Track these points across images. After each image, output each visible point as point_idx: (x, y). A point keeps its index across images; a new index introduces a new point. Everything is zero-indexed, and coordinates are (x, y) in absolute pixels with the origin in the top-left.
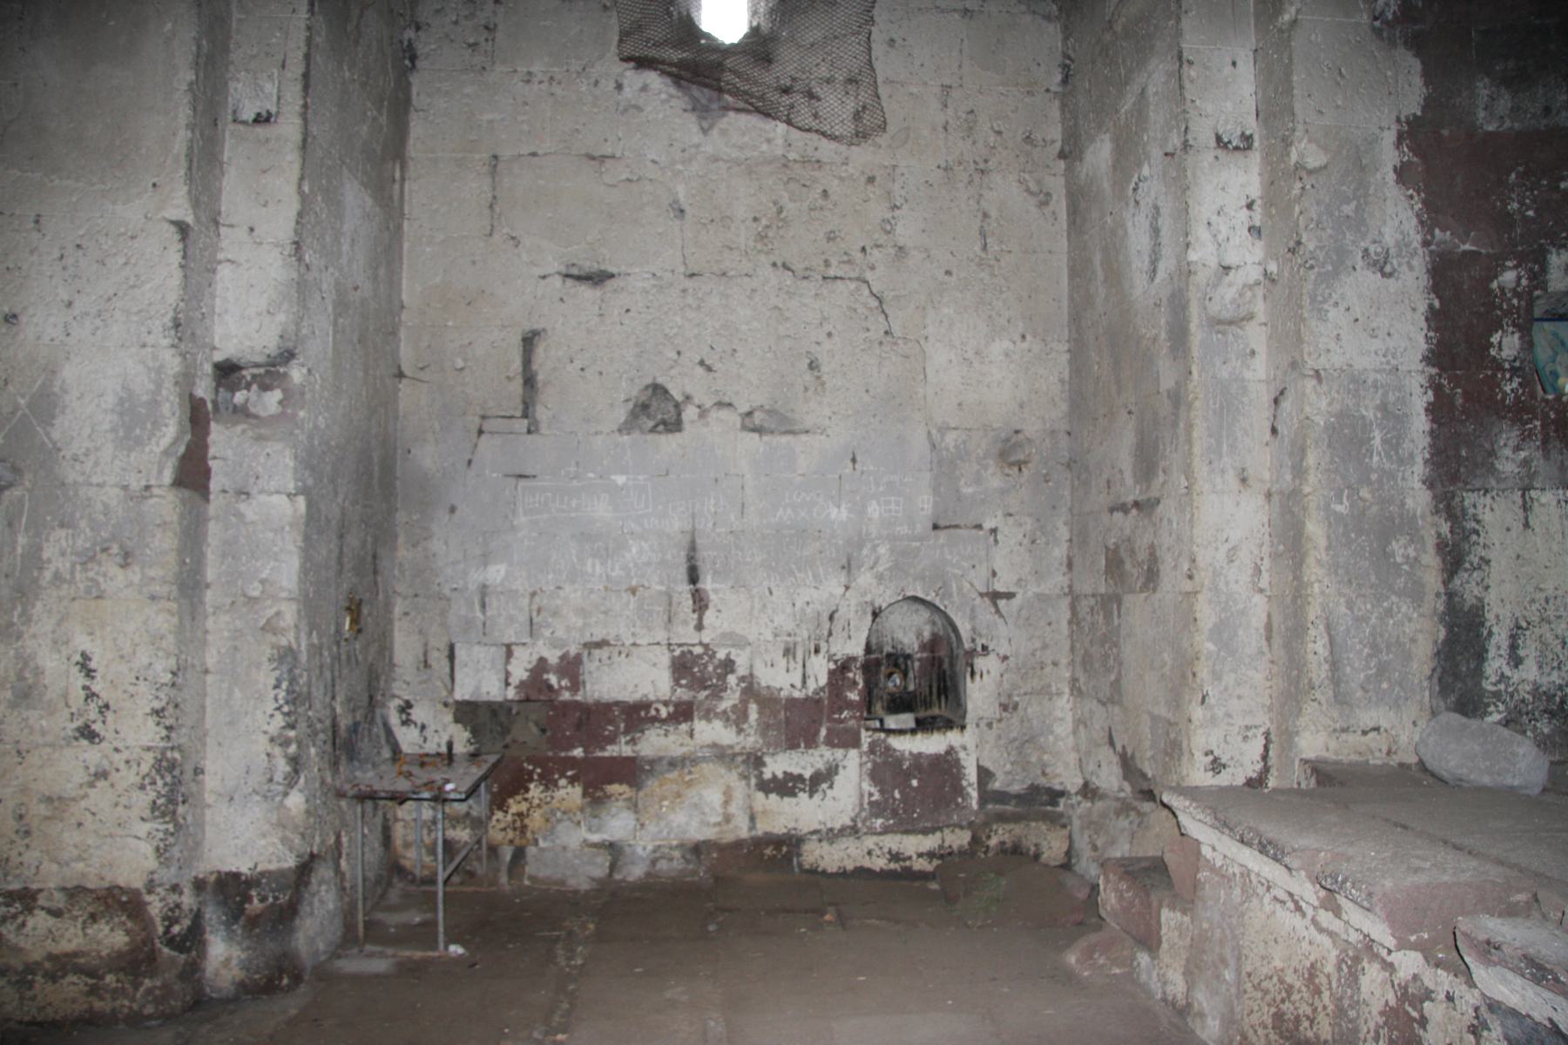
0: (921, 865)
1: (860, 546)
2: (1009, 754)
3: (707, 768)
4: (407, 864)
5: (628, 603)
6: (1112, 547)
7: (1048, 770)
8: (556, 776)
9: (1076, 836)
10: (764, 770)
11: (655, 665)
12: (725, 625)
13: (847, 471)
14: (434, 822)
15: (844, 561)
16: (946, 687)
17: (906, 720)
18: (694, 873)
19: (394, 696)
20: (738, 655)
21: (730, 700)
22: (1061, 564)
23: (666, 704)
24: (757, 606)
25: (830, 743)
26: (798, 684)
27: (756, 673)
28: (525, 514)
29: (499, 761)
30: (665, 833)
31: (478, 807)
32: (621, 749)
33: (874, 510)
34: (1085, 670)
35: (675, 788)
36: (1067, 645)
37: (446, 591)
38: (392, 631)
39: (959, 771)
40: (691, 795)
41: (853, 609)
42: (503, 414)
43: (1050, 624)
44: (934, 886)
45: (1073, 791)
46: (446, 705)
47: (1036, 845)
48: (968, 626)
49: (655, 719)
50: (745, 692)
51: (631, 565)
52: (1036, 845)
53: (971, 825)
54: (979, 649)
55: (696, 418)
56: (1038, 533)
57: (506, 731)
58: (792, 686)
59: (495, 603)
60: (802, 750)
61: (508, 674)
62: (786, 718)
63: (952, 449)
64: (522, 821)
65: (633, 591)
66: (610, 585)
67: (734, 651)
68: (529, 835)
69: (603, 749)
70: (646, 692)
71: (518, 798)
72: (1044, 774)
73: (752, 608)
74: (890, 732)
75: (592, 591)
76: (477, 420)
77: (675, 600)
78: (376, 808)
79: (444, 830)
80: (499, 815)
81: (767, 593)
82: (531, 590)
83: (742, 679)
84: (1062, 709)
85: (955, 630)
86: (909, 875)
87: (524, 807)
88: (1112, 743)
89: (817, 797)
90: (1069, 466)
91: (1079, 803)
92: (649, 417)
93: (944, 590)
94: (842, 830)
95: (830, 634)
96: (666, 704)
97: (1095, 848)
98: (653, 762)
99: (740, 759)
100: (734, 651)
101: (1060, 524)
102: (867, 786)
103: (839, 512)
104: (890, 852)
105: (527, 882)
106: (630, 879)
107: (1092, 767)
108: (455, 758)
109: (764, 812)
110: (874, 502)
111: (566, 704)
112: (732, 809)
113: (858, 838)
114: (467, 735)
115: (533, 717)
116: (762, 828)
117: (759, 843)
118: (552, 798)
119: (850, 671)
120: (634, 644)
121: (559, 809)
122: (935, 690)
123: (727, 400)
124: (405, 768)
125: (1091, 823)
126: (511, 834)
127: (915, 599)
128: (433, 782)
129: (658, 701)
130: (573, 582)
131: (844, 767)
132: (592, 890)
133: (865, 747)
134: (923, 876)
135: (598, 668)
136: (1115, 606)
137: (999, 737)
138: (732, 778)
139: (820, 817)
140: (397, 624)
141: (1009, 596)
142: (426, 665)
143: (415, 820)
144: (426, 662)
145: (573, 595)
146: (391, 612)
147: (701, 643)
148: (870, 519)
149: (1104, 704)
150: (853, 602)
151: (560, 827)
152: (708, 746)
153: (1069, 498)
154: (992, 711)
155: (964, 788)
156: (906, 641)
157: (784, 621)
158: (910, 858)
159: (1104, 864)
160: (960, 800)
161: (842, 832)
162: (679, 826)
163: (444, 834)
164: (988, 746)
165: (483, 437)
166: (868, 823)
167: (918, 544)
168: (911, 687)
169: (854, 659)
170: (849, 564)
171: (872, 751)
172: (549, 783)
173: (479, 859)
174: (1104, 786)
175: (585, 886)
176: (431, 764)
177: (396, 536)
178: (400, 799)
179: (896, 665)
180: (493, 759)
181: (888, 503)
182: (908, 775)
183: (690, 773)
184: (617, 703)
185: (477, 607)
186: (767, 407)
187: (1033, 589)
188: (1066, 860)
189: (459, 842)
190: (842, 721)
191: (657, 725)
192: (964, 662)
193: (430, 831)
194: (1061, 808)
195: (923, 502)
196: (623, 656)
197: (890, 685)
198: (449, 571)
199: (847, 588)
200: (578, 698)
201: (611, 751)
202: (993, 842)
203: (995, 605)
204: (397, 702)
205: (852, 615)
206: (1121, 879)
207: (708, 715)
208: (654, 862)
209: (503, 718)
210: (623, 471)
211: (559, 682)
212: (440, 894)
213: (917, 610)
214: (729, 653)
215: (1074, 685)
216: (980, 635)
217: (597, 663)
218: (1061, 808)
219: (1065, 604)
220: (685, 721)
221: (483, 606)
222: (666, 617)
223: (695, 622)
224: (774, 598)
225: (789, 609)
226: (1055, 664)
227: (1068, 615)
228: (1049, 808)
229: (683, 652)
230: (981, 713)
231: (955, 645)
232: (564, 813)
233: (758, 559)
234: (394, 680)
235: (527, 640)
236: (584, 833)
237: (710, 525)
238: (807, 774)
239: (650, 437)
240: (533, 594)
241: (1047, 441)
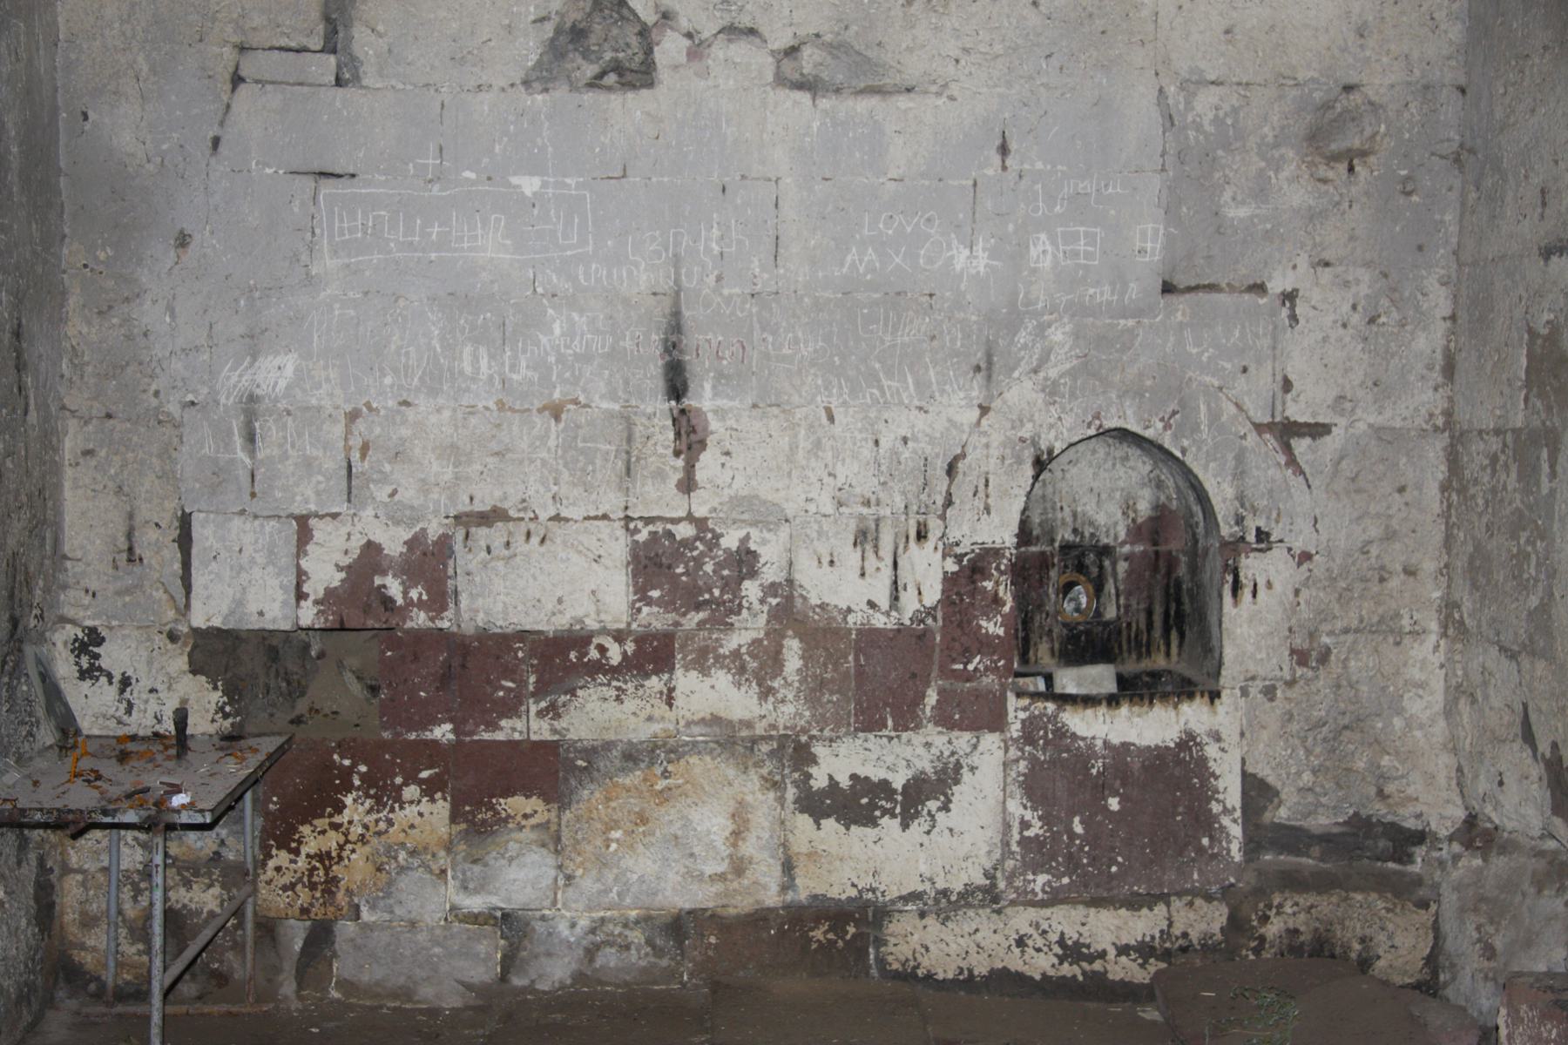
0: (1124, 970)
1: (1013, 327)
2: (1308, 752)
3: (697, 764)
4: (87, 959)
5: (544, 437)
6: (1545, 331)
7: (1390, 788)
8: (399, 780)
9: (1448, 927)
10: (813, 770)
11: (597, 559)
12: (739, 482)
13: (990, 172)
14: (147, 874)
15: (980, 356)
16: (1180, 616)
17: (1100, 678)
18: (671, 974)
19: (64, 620)
20: (764, 542)
21: (746, 631)
22: (1430, 368)
23: (619, 637)
24: (804, 444)
25: (945, 720)
26: (884, 602)
27: (798, 577)
28: (335, 253)
29: (281, 750)
30: (614, 895)
31: (237, 842)
32: (530, 726)
33: (1042, 252)
34: (1475, 586)
35: (635, 804)
36: (1438, 535)
37: (173, 408)
38: (58, 487)
39: (1204, 783)
40: (668, 818)
41: (995, 452)
42: (284, 42)
43: (1401, 490)
44: (1151, 1014)
45: (1443, 833)
46: (173, 637)
47: (1363, 940)
48: (1230, 492)
49: (598, 668)
50: (776, 614)
51: (552, 359)
52: (1363, 940)
53: (1227, 892)
54: (1251, 537)
55: (683, 59)
56: (1385, 302)
57: (296, 690)
58: (872, 604)
59: (275, 434)
61: (301, 576)
62: (859, 668)
63: (1209, 128)
64: (327, 870)
65: (556, 412)
66: (508, 401)
67: (755, 534)
68: (340, 896)
69: (493, 726)
70: (580, 612)
71: (321, 823)
72: (1381, 793)
73: (793, 448)
74: (1066, 700)
75: (472, 410)
76: (228, 53)
77: (638, 430)
78: (23, 845)
79: (166, 890)
80: (281, 858)
81: (824, 420)
82: (348, 408)
83: (772, 589)
84: (1424, 662)
85: (1203, 498)
86: (1100, 989)
87: (332, 841)
88: (1528, 737)
90: (1457, 160)
91: (1456, 858)
92: (586, 55)
93: (1181, 416)
94: (967, 893)
95: (949, 502)
96: (619, 637)
97: (1489, 952)
98: (592, 752)
99: (765, 748)
100: (755, 534)
101: (1432, 283)
102: (1015, 807)
103: (972, 257)
104: (1061, 942)
105: (335, 994)
106: (543, 986)
107: (1483, 785)
108: (191, 744)
109: (812, 855)
110: (1043, 236)
111: (419, 636)
112: (748, 848)
113: (999, 912)
114: (216, 697)
115: (353, 662)
116: (807, 886)
117: (800, 917)
118: (390, 823)
119: (989, 577)
120: (557, 518)
121: (403, 845)
122: (1158, 619)
123: (745, 21)
124: (86, 764)
125: (1482, 899)
126: (304, 896)
127: (1123, 435)
128: (146, 790)
129: (604, 631)
130: (434, 392)
131: (973, 769)
132: (467, 1008)
133: (1015, 730)
134: (1128, 992)
135: (485, 565)
136: (1545, 454)
137: (1290, 717)
138: (750, 787)
139: (923, 868)
140: (69, 472)
141: (1318, 430)
142: (132, 556)
143: (105, 870)
144: (131, 550)
145: (433, 419)
146: (56, 450)
147: (690, 518)
148: (1034, 271)
149: (1513, 656)
150: (996, 438)
151: (404, 882)
152: (703, 721)
153: (1454, 229)
154: (1274, 663)
155: (1216, 818)
156: (1101, 519)
157: (856, 474)
158: (1103, 955)
159: (1509, 986)
160: (1205, 841)
161: (967, 898)
162: (641, 880)
163: (166, 899)
164: (1265, 735)
165: (242, 88)
166: (1018, 883)
167: (1131, 323)
168: (1111, 613)
169: (996, 553)
170: (990, 363)
171: (1028, 737)
172: (383, 793)
173: (238, 947)
174: (1510, 825)
175: (452, 1000)
176: (140, 755)
177: (64, 294)
178: (75, 826)
179: (1081, 568)
180: (269, 745)
181: (1072, 238)
182: (1101, 788)
183: (666, 774)
184: (522, 635)
185: (238, 441)
186: (828, 38)
187: (1368, 418)
188: (1426, 975)
189: (198, 913)
190: (968, 677)
191: (601, 678)
192: (1219, 563)
193: (137, 892)
194: (1416, 867)
195: (1144, 234)
196: (535, 540)
197: (1068, 607)
198: (177, 365)
199: (984, 410)
200: (445, 624)
201: (509, 729)
202: (1274, 929)
203: (1287, 449)
204: (71, 631)
206: (1544, 1017)
207: (703, 661)
208: (591, 952)
209: (292, 665)
210: (534, 167)
211: (405, 593)
212: (156, 1018)
213: (1126, 458)
214: (747, 537)
215: (1449, 616)
216: (1255, 511)
217: (484, 554)
218: (1416, 867)
219: (1434, 451)
220: (657, 672)
221: (251, 438)
222: (620, 465)
223: (679, 475)
224: (837, 429)
225: (867, 451)
226: (1410, 572)
227: (1441, 471)
228: (1391, 865)
229: (653, 534)
230: (1252, 668)
231: (1201, 530)
232: (413, 853)
233: (806, 351)
234: (65, 587)
235: (340, 507)
236: (451, 893)
237: (711, 280)
238: (898, 782)
239: (589, 97)
240: (353, 416)
241: (1413, 108)
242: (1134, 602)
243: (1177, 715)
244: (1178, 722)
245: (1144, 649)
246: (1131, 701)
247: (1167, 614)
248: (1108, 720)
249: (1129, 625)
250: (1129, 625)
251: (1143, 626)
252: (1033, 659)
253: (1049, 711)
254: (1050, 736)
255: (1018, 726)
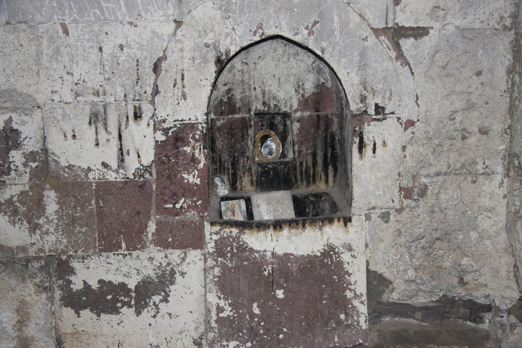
2: (412, 256)
10: (73, 278)
16: (334, 157)
20: (23, 123)
26: (114, 163)
39: (341, 278)
41: (187, 55)
43: (479, 74)
48: (356, 79)
50: (35, 174)
54: (371, 111)
58: (105, 165)
60: (123, 251)
67: (15, 117)
72: (462, 282)
83: (31, 156)
89: (146, 314)
95: (156, 92)
100: (15, 117)
102: (213, 298)
109: (76, 334)
112: (30, 331)
119: (188, 144)
122: (320, 159)
131: (183, 274)
133: (211, 247)
137: (399, 233)
150: (188, 45)
155: (349, 301)
156: (281, 95)
160: (342, 316)
164: (382, 246)
171: (220, 251)
194: (485, 326)
199: (178, 23)
203: (397, 47)
205: (186, 64)
214: (10, 119)
216: (374, 92)
218: (485, 326)
224: (71, 39)
225: (94, 55)
226: (483, 132)
230: (373, 202)
242: (304, 149)
243: (322, 234)
244: (322, 239)
245: (311, 179)
246: (290, 225)
247: (325, 156)
248: (275, 239)
249: (301, 163)
250: (301, 163)
251: (310, 164)
252: (239, 187)
253: (234, 234)
254: (235, 251)
255: (213, 244)
